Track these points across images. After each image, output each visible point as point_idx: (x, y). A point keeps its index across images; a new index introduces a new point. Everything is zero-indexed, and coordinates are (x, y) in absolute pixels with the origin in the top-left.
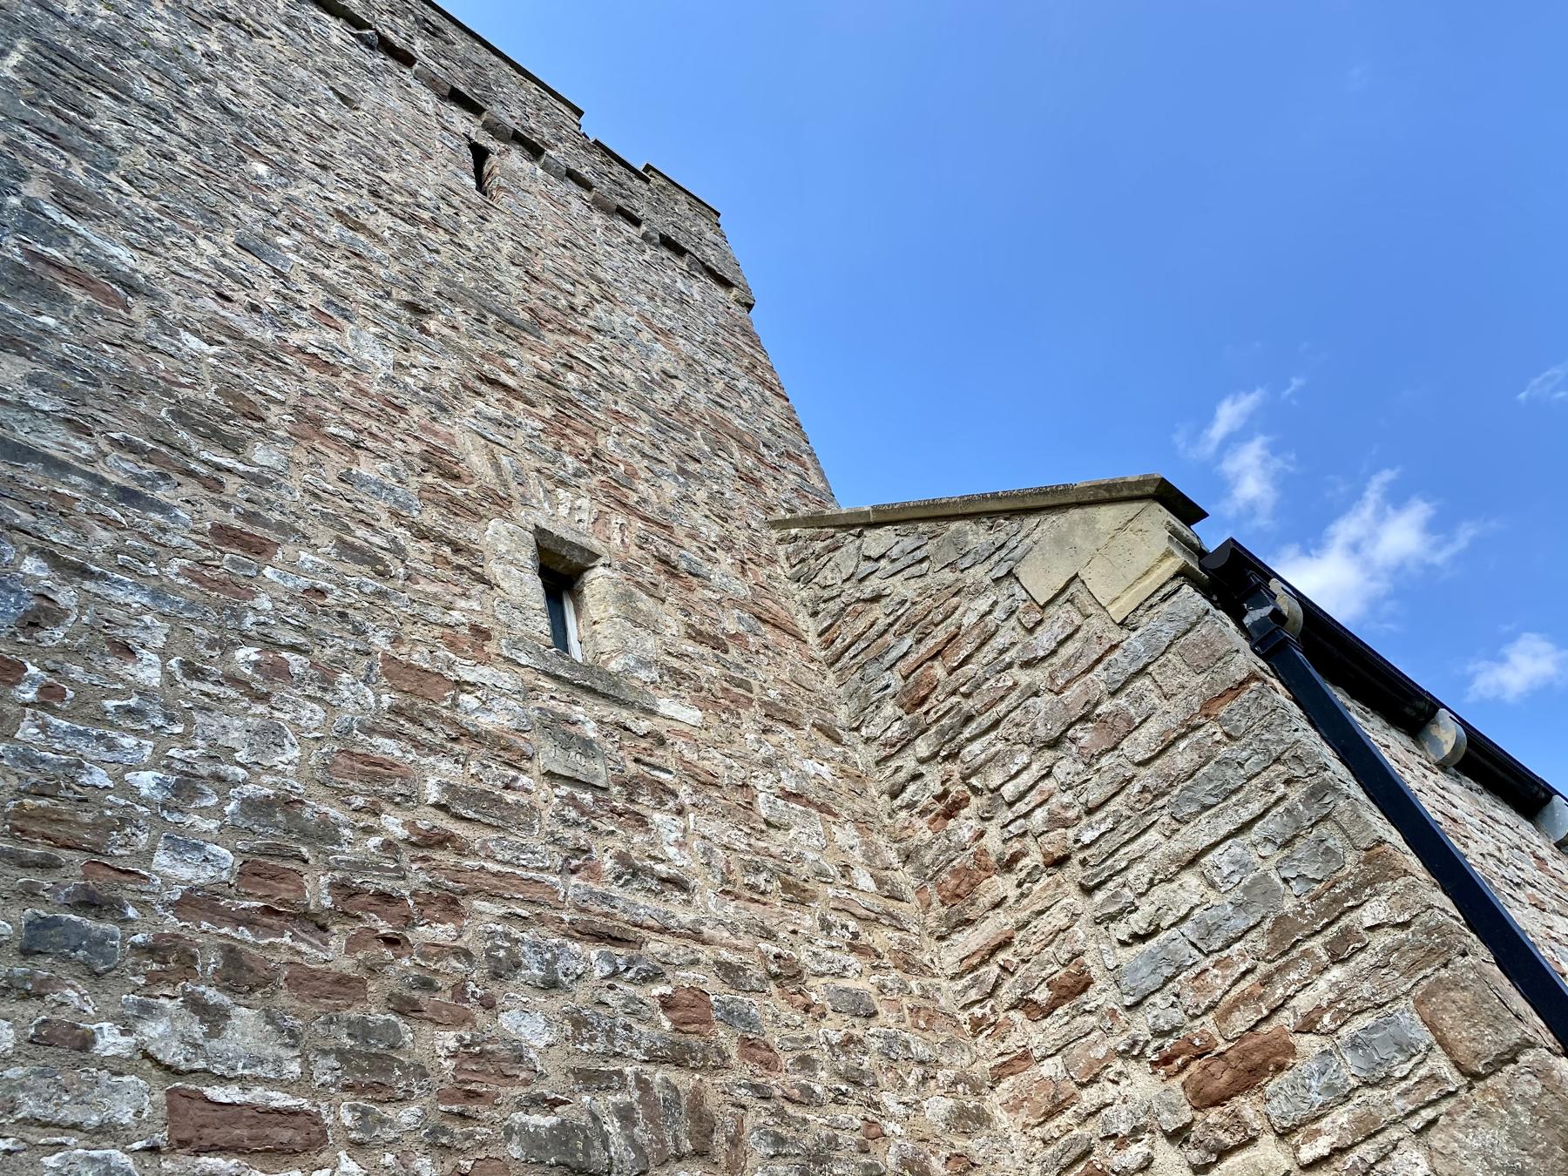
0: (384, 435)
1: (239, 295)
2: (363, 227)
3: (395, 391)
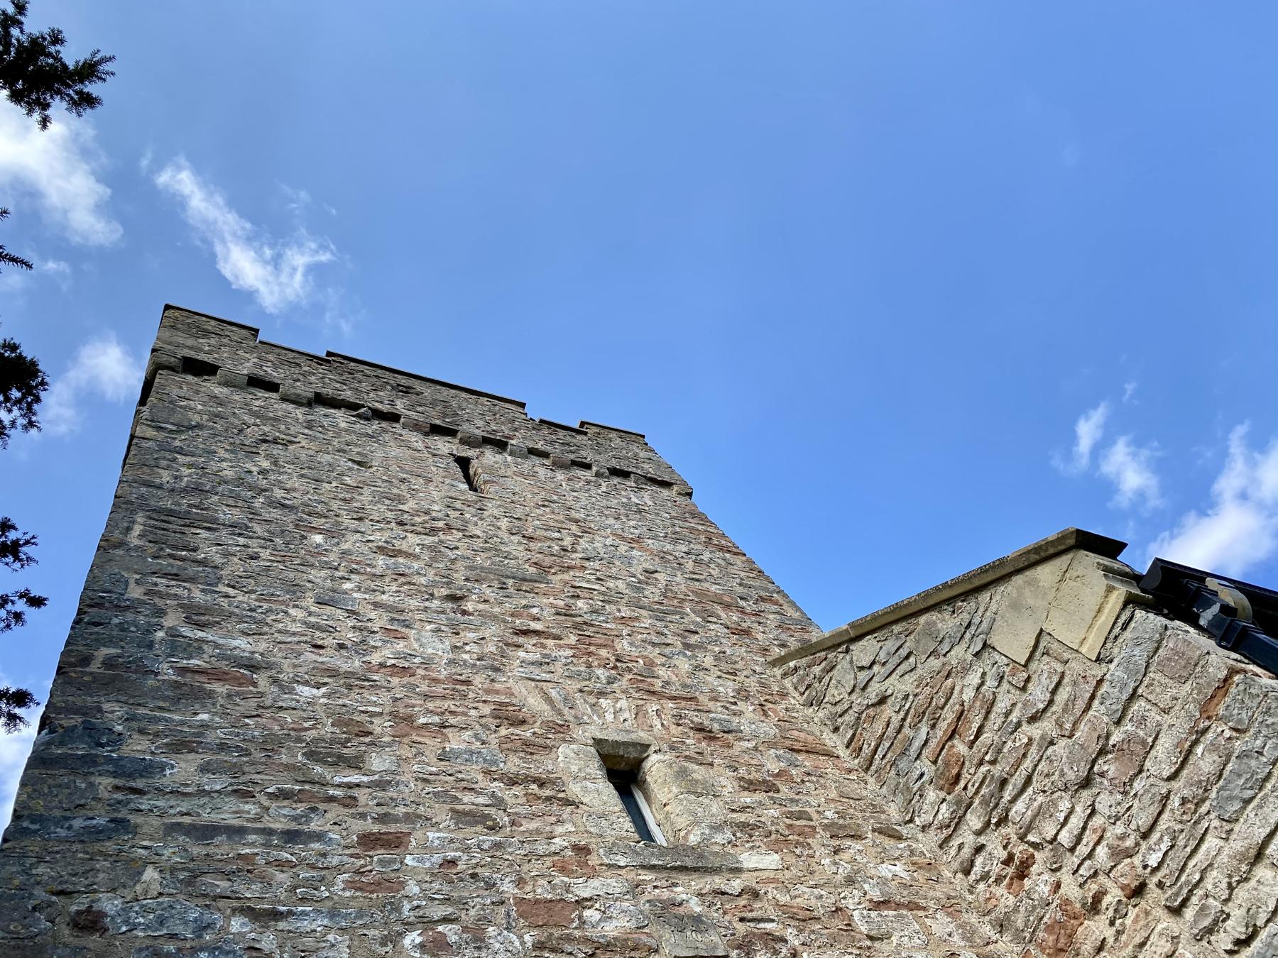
0: (460, 710)
1: (329, 641)
2: (400, 551)
3: (458, 670)
